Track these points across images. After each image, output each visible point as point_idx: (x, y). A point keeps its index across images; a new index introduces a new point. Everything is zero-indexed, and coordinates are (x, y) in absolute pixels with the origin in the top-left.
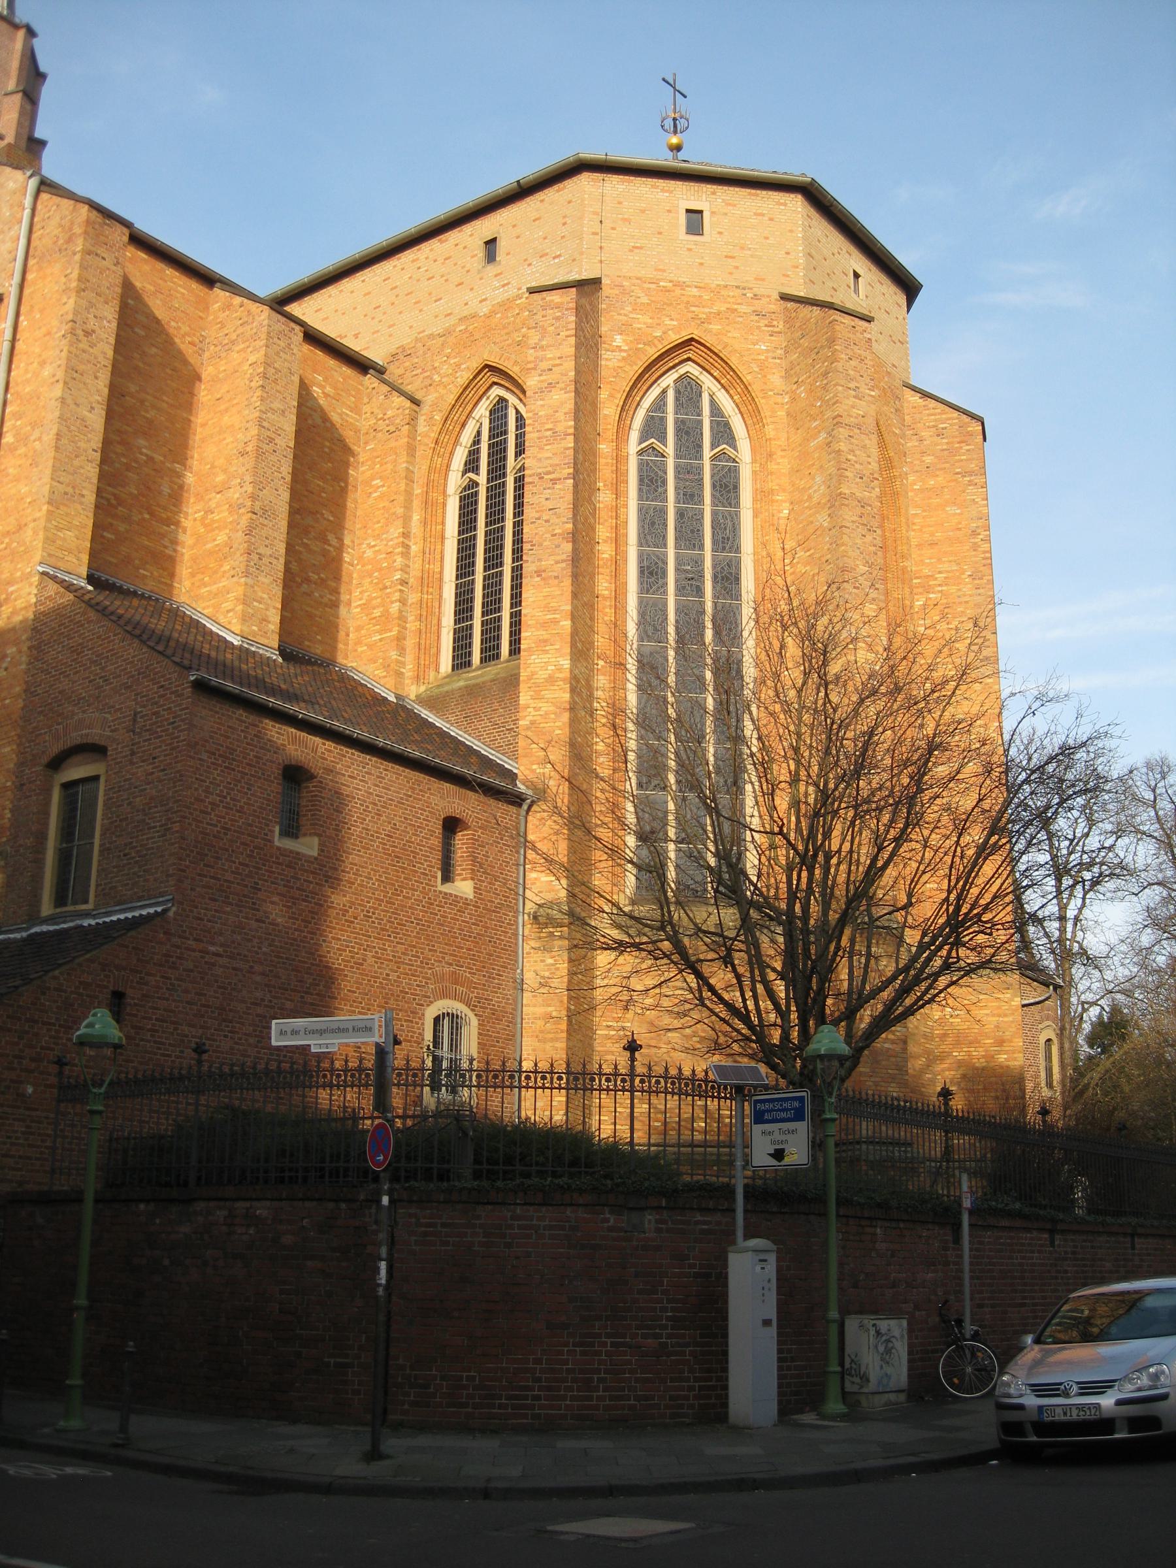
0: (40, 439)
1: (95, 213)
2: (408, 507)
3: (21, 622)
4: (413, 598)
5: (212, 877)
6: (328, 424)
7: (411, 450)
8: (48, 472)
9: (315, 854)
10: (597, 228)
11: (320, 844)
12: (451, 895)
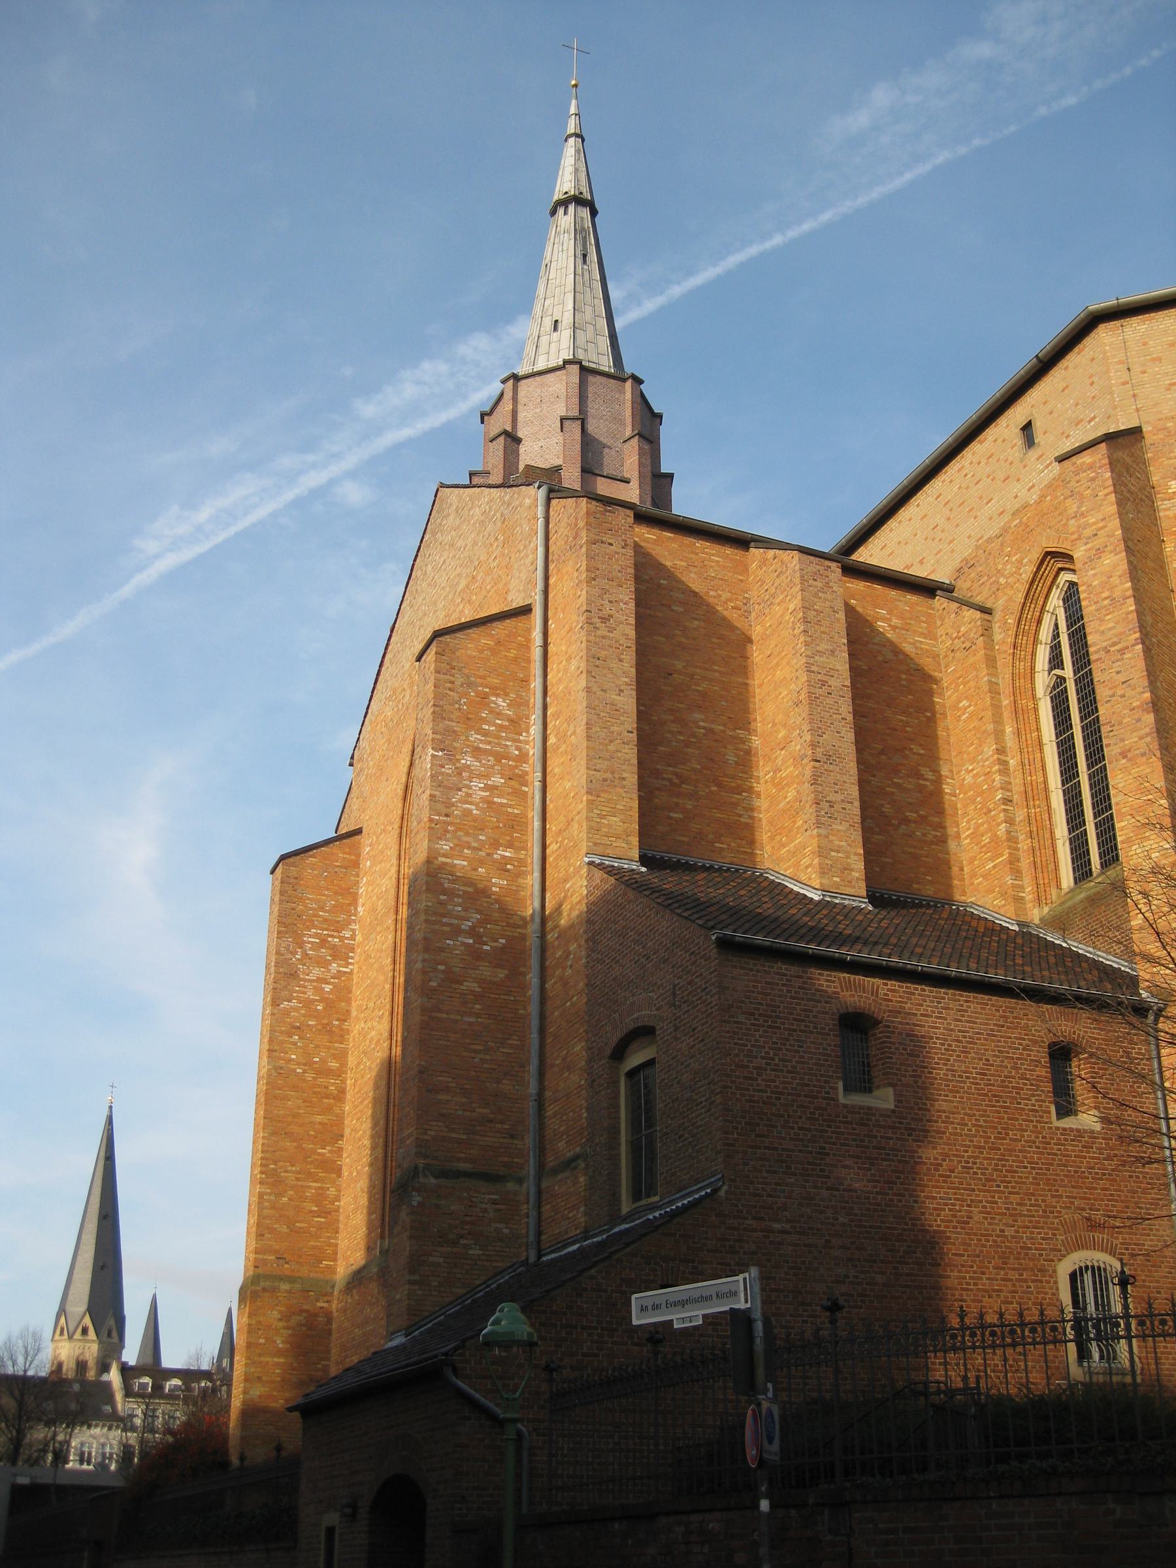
0: (574, 733)
1: (594, 503)
2: (998, 720)
3: (578, 917)
4: (1020, 815)
5: (766, 1148)
6: (901, 657)
7: (991, 661)
8: (584, 762)
9: (892, 1107)
10: (1125, 376)
11: (895, 1095)
12: (1071, 1130)
